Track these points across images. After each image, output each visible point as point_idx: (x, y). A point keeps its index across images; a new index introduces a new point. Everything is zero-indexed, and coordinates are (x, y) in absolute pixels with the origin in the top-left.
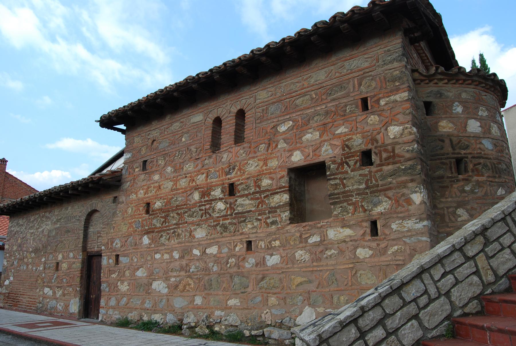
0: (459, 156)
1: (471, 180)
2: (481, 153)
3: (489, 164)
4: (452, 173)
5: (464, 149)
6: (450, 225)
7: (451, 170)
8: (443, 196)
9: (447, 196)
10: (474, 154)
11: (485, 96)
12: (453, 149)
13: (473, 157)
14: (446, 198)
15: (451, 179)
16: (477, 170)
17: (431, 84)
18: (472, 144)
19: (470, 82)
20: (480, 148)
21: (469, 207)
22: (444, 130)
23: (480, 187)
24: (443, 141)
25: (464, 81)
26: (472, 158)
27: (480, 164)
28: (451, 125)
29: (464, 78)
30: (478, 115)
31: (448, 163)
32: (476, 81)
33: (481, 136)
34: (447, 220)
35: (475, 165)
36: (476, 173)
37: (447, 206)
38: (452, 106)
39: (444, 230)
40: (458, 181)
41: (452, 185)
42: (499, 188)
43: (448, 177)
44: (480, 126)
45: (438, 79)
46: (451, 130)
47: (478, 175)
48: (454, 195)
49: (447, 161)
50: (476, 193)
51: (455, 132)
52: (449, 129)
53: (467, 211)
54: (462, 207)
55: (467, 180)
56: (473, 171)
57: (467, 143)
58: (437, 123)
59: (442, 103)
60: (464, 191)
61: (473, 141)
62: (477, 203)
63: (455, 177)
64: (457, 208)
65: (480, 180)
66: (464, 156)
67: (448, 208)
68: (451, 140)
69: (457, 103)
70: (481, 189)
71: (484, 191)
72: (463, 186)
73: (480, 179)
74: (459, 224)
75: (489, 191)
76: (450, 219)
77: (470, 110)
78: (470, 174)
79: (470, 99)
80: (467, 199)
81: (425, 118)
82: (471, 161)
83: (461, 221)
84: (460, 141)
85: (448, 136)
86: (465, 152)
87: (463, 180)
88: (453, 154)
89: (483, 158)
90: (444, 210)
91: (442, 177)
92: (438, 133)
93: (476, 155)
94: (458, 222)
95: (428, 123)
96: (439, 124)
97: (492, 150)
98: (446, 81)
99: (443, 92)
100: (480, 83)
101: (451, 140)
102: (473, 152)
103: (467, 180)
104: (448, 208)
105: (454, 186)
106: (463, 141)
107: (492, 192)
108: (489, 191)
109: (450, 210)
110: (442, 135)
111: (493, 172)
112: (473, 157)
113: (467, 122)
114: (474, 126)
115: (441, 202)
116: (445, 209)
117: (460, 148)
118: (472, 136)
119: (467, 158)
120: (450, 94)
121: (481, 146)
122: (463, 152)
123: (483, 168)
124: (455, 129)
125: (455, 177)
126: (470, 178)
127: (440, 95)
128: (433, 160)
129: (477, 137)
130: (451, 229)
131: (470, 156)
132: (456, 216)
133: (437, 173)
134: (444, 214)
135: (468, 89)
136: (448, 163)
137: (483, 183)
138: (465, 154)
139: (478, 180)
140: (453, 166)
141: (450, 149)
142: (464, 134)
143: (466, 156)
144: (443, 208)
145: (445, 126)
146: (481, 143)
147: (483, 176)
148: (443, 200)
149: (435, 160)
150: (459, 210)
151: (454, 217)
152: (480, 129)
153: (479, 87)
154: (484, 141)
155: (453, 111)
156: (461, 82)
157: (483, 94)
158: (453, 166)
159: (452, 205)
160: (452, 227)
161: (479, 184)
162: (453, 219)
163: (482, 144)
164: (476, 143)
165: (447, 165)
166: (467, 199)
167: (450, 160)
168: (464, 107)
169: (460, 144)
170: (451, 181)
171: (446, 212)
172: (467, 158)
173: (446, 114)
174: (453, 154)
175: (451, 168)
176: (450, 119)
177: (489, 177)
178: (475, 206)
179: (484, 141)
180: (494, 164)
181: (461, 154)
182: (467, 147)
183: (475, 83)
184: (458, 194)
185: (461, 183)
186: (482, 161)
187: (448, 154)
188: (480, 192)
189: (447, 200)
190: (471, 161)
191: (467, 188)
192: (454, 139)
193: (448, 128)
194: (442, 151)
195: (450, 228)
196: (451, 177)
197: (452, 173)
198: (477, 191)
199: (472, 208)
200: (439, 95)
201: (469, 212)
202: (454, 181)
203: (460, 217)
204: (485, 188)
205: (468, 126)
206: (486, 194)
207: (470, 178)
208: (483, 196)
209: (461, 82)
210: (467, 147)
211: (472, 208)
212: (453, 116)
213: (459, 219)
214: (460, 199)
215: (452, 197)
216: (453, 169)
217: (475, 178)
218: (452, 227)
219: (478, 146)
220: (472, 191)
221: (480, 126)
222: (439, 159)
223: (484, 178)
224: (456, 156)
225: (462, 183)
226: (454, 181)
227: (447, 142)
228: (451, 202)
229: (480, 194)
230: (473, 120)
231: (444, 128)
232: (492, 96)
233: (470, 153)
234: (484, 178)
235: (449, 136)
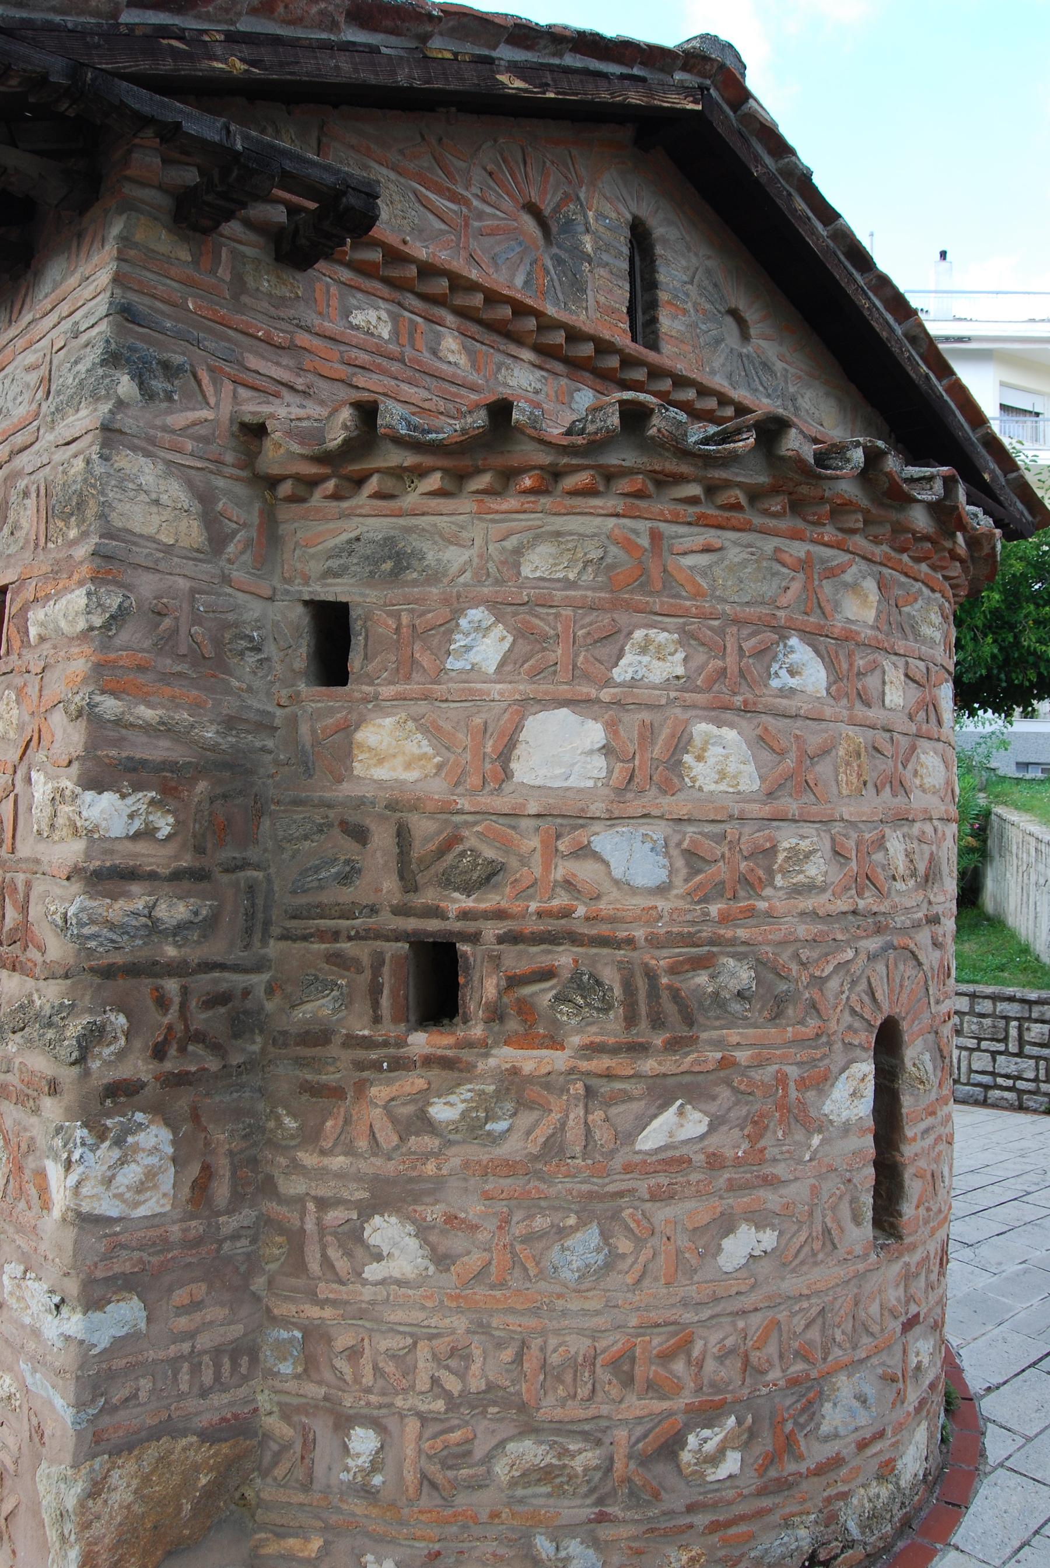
0: (433, 925)
1: (470, 1067)
2: (566, 913)
3: (610, 976)
4: (377, 1020)
5: (468, 889)
6: (324, 1290)
7: (376, 1005)
8: (310, 1137)
9: (327, 1144)
10: (524, 915)
11: (707, 550)
12: (409, 884)
13: (513, 938)
14: (323, 1153)
15: (360, 1054)
16: (526, 1010)
17: (362, 499)
18: (524, 861)
19: (582, 479)
20: (568, 884)
21: (433, 1213)
22: (381, 773)
23: (523, 1104)
24: (360, 835)
25: (556, 474)
26: (501, 940)
27: (547, 974)
28: (419, 745)
29: (545, 458)
30: (608, 682)
31: (366, 961)
32: (629, 472)
33: (597, 808)
34: (314, 1266)
35: (514, 982)
36: (513, 1025)
37: (321, 1192)
38: (449, 627)
39: (293, 1309)
40: (400, 1064)
41: (361, 1087)
42: (664, 1107)
43: (353, 1042)
44: (607, 750)
45: (398, 473)
46: (412, 775)
47: (527, 1041)
48: (362, 1144)
49: (361, 951)
50: (496, 1139)
51: (437, 789)
52: (408, 766)
53: (422, 1231)
54: (398, 1211)
55: (447, 1064)
56: (496, 1015)
57: (489, 853)
58: (348, 729)
59: (397, 616)
60: (424, 1123)
61: (535, 842)
62: (487, 1196)
63: (386, 1044)
64: (367, 1210)
65: (528, 1067)
66: (458, 926)
67: (323, 1204)
68: (403, 834)
69: (477, 614)
70: (526, 1119)
71: (541, 1134)
72: (423, 1098)
73: (531, 1061)
74: (367, 1293)
75: (574, 1134)
76: (327, 1262)
77: (559, 653)
78: (477, 1031)
79: (572, 585)
80: (430, 1168)
81: (295, 698)
82: (496, 960)
83: (383, 1282)
84: (455, 839)
85: (392, 806)
86: (468, 903)
87: (428, 1061)
88: (402, 911)
89: (574, 939)
90: (303, 1213)
91: (318, 1036)
92: (347, 790)
93: (532, 926)
94: (365, 1283)
95: (304, 729)
96: (360, 736)
97: (661, 890)
98: (434, 481)
99: (416, 542)
100: (663, 481)
101: (403, 834)
102: (516, 907)
103: (447, 1064)
104: (323, 1204)
105: (374, 1091)
106: (472, 842)
107: (602, 1135)
108: (574, 1134)
109: (335, 1216)
110: (360, 803)
111: (631, 1020)
112: (513, 938)
113: (518, 728)
114: (561, 751)
115: (296, 1167)
116: (311, 1206)
117: (447, 882)
118: (533, 808)
119: (474, 938)
120: (455, 557)
121: (585, 871)
122: (459, 902)
123: (561, 998)
124: (440, 767)
125: (386, 1044)
126: (466, 1055)
127: (395, 561)
128: (294, 939)
129: (565, 821)
130: (328, 1313)
131: (491, 930)
132: (359, 1252)
133: (305, 1012)
134: (302, 1231)
135: (574, 524)
136: (366, 961)
137: (547, 1086)
138: (465, 915)
139: (515, 1071)
140: (386, 978)
141: (390, 885)
142: (487, 801)
143: (471, 927)
144: (299, 1201)
145: (390, 752)
146: (584, 852)
147: (555, 1043)
148: (308, 1159)
149: (305, 938)
150: (377, 1220)
151: (348, 1254)
152: (599, 763)
153: (662, 506)
154: (607, 842)
155: (451, 663)
156: (527, 482)
157: (687, 543)
158: (386, 978)
159: (346, 1195)
160: (334, 1303)
161: (514, 1087)
162: (342, 1265)
163: (596, 856)
164: (551, 853)
165: (360, 971)
166: (430, 1168)
167: (380, 944)
168: (523, 633)
169: (450, 858)
170: (360, 1066)
171: (310, 1226)
172: (474, 938)
173: (408, 678)
174: (402, 911)
175: (375, 991)
176: (423, 707)
177: (594, 1049)
178: (474, 1209)
179: (607, 842)
180: (651, 976)
181: (437, 913)
182: (490, 876)
183: (624, 485)
184: (388, 1137)
185: (415, 1082)
186: (564, 958)
187: (373, 910)
188: (517, 1135)
189: (326, 1161)
190: (496, 960)
191: (444, 1111)
192: (425, 829)
193: (399, 760)
194: (346, 895)
195: (322, 1303)
196: (367, 1043)
197: (377, 1020)
198: (498, 1126)
199: (451, 1219)
200: (388, 566)
201: (433, 1238)
202: (376, 1066)
203: (378, 1257)
204: (555, 1116)
205: (520, 750)
206: (553, 1147)
207: (466, 1055)
208: (536, 1158)
209: (527, 482)
210: (490, 876)
211: (451, 1219)
212: (439, 689)
213: (373, 1271)
214: (390, 1168)
215: (350, 1151)
216: (385, 1001)
217: (504, 1056)
218: (334, 1303)
219: (561, 870)
220: (472, 1128)
221: (607, 750)
222: (322, 935)
223: (559, 1060)
224: (412, 924)
225: (421, 1083)
226: (376, 1066)
227: (382, 838)
228: (340, 1175)
229: (513, 1148)
230: (564, 711)
231: (381, 761)
232: (769, 544)
233: (500, 915)
234: (559, 1060)
235: (398, 807)
